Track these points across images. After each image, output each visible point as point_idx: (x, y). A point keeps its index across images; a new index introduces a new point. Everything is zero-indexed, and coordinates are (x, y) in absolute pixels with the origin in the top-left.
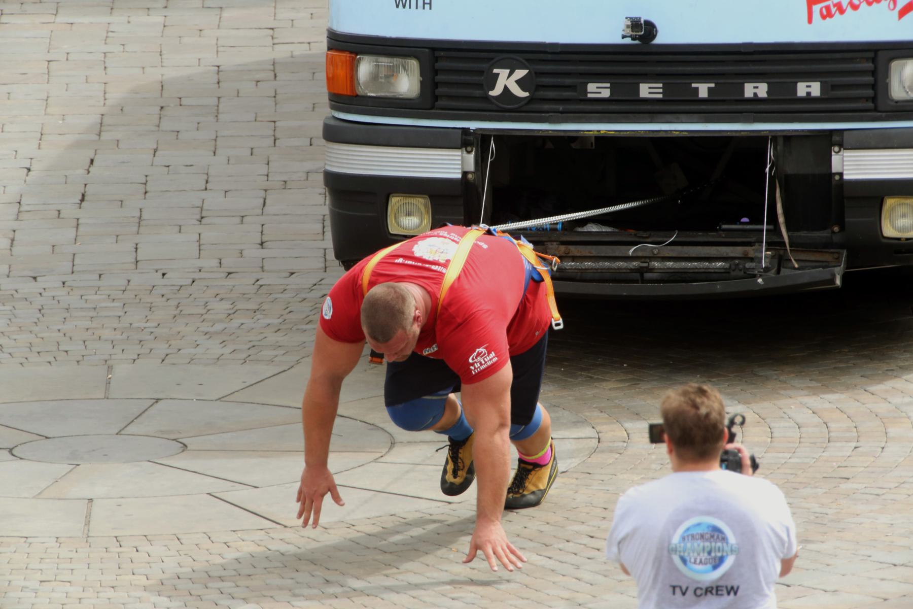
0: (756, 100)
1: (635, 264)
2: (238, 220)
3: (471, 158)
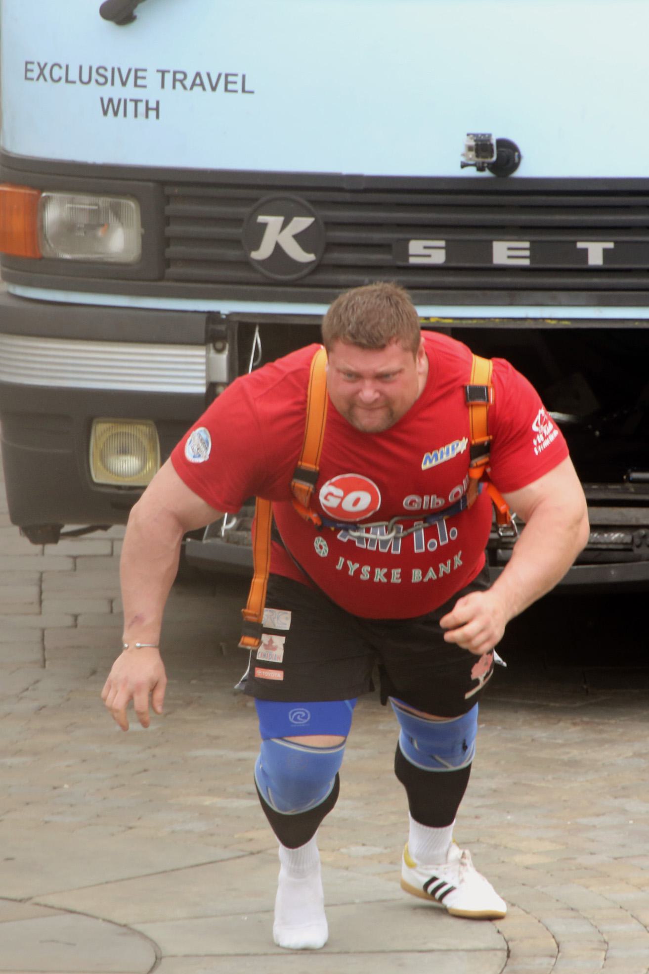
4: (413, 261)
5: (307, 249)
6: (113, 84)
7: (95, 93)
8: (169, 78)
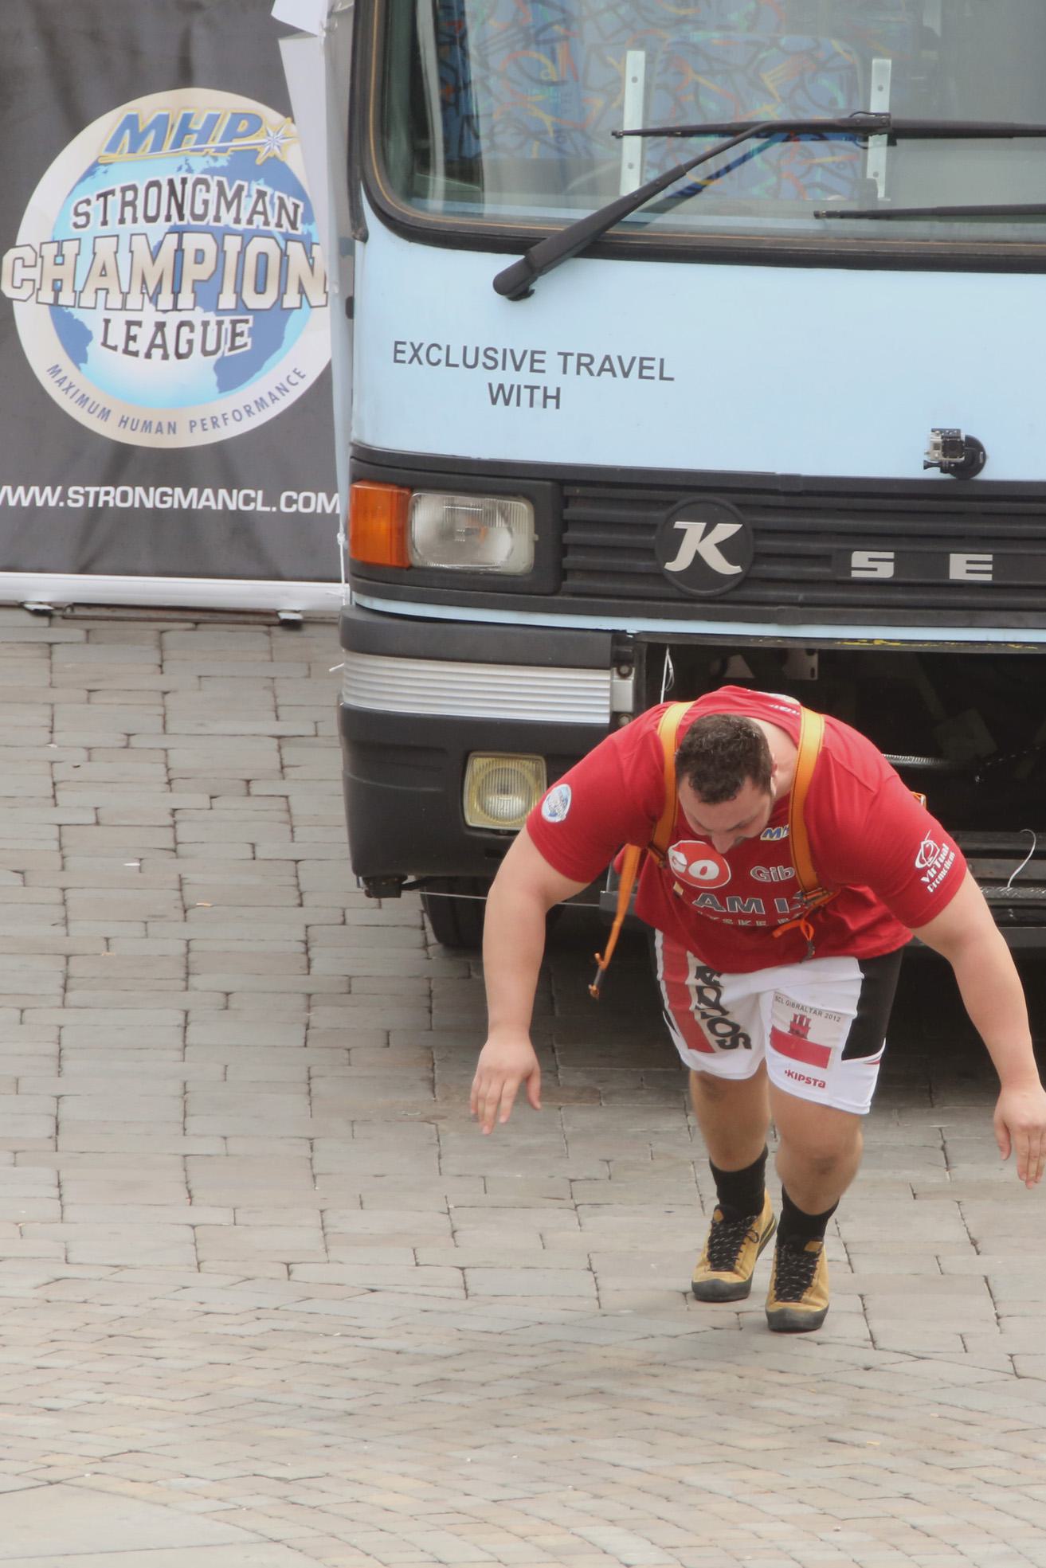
3: (627, 686)
4: (855, 574)
5: (732, 561)
6: (504, 368)
7: (482, 378)
8: (572, 362)
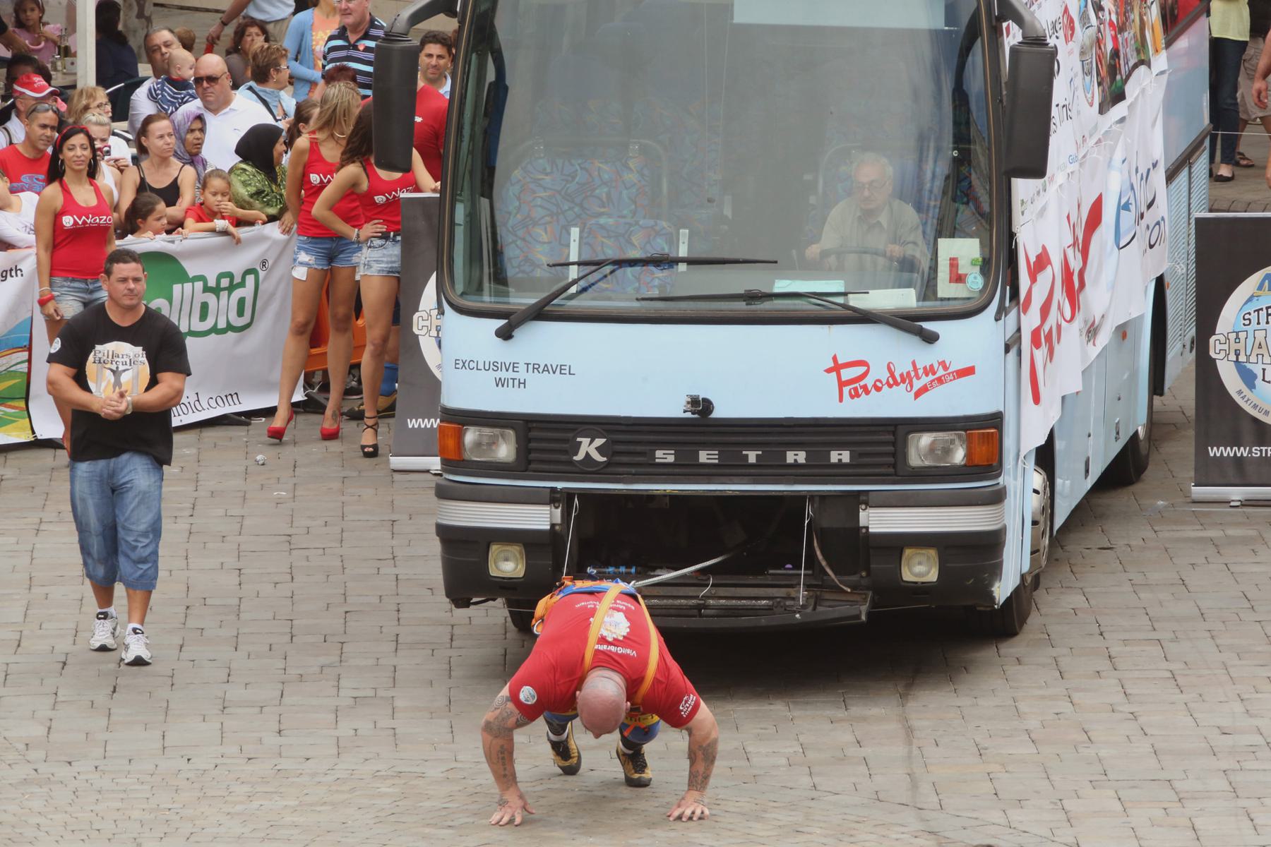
0: (796, 465)
1: (694, 602)
2: (257, 710)
7: (492, 375)
8: (531, 367)
